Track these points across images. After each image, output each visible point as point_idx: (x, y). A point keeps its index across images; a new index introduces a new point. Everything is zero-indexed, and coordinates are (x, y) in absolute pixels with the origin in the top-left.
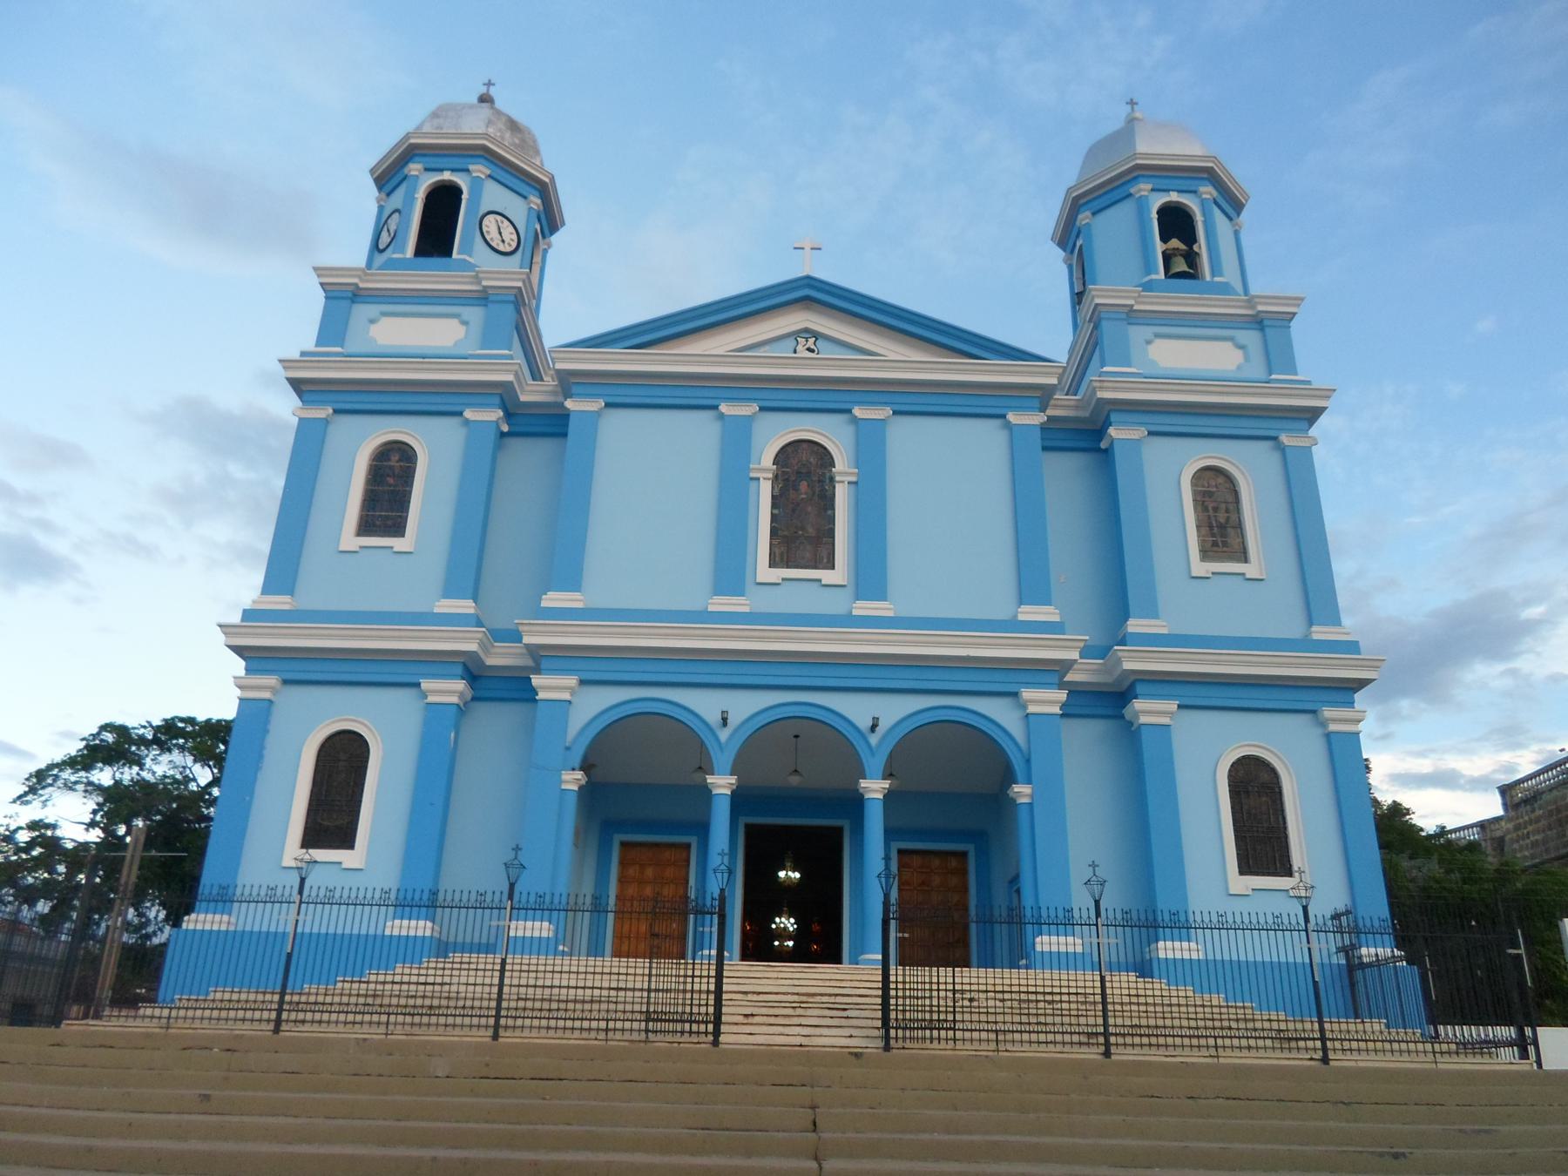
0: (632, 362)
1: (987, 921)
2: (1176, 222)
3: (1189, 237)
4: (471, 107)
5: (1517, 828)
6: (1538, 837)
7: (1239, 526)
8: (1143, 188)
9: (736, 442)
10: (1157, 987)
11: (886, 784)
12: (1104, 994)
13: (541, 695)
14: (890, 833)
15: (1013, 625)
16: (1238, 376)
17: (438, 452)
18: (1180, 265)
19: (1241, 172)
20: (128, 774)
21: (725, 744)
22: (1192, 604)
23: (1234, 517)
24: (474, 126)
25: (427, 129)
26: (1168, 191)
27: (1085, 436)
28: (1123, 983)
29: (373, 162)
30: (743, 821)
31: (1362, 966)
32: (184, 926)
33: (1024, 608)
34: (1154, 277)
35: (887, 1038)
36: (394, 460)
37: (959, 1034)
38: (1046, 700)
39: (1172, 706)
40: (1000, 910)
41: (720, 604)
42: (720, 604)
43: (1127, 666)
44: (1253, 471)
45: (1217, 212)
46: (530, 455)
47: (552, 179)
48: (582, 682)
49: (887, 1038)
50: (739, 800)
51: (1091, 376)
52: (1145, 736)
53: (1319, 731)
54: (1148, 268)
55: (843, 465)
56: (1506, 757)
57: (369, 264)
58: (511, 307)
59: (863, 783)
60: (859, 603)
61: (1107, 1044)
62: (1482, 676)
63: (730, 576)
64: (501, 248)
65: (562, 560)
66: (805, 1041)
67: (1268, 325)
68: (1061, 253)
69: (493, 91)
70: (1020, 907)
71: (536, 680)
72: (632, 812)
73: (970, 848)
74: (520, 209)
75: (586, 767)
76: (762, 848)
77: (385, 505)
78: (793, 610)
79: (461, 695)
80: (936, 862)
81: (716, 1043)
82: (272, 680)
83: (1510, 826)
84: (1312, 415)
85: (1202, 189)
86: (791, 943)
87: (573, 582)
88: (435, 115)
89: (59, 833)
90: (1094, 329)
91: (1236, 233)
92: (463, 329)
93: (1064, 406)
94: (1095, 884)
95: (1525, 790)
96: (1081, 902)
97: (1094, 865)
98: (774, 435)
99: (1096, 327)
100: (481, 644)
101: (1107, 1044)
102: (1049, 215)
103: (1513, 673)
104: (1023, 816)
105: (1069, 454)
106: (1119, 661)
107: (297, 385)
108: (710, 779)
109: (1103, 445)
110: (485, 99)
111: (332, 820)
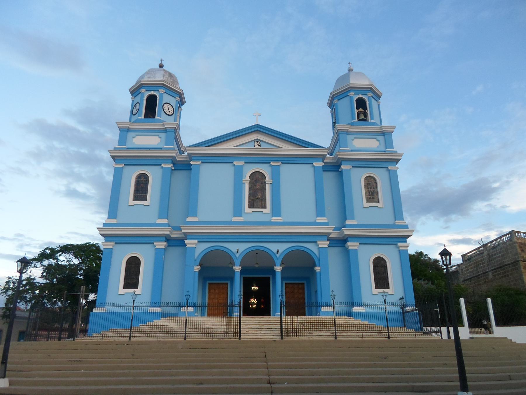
0: (208, 150)
1: (310, 306)
2: (361, 104)
3: (365, 108)
4: (156, 70)
5: (466, 267)
6: (471, 270)
7: (377, 193)
8: (352, 94)
10: (352, 319)
11: (281, 268)
12: (335, 322)
14: (283, 279)
15: (315, 223)
17: (155, 176)
18: (362, 117)
19: (379, 87)
20: (53, 262)
21: (238, 258)
22: (365, 215)
23: (375, 190)
24: (159, 77)
25: (146, 78)
27: (335, 167)
28: (342, 319)
30: (242, 276)
32: (94, 311)
33: (318, 218)
34: (354, 121)
35: (282, 335)
37: (299, 334)
38: (324, 244)
39: (358, 244)
40: (313, 301)
41: (236, 219)
42: (236, 219)
43: (346, 233)
45: (372, 99)
46: (181, 175)
47: (182, 91)
48: (198, 242)
49: (282, 335)
50: (242, 272)
51: (336, 151)
52: (351, 252)
53: (397, 249)
55: (268, 179)
56: (487, 234)
57: (130, 120)
59: (275, 268)
60: (273, 218)
61: (336, 335)
62: (480, 206)
64: (169, 114)
65: (191, 207)
67: (386, 134)
71: (186, 242)
72: (213, 275)
73: (305, 282)
74: (173, 101)
76: (247, 283)
77: (141, 193)
78: (255, 220)
79: (165, 246)
80: (296, 286)
81: (240, 339)
82: (113, 243)
83: (464, 267)
84: (397, 161)
85: (368, 94)
87: (195, 214)
88: (147, 73)
89: (35, 281)
91: (379, 105)
92: (160, 139)
93: (329, 159)
95: (490, 246)
98: (249, 170)
99: (338, 136)
100: (170, 232)
101: (336, 335)
103: (490, 205)
104: (318, 275)
105: (329, 173)
107: (113, 157)
109: (340, 170)
110: (161, 66)
111: (131, 281)
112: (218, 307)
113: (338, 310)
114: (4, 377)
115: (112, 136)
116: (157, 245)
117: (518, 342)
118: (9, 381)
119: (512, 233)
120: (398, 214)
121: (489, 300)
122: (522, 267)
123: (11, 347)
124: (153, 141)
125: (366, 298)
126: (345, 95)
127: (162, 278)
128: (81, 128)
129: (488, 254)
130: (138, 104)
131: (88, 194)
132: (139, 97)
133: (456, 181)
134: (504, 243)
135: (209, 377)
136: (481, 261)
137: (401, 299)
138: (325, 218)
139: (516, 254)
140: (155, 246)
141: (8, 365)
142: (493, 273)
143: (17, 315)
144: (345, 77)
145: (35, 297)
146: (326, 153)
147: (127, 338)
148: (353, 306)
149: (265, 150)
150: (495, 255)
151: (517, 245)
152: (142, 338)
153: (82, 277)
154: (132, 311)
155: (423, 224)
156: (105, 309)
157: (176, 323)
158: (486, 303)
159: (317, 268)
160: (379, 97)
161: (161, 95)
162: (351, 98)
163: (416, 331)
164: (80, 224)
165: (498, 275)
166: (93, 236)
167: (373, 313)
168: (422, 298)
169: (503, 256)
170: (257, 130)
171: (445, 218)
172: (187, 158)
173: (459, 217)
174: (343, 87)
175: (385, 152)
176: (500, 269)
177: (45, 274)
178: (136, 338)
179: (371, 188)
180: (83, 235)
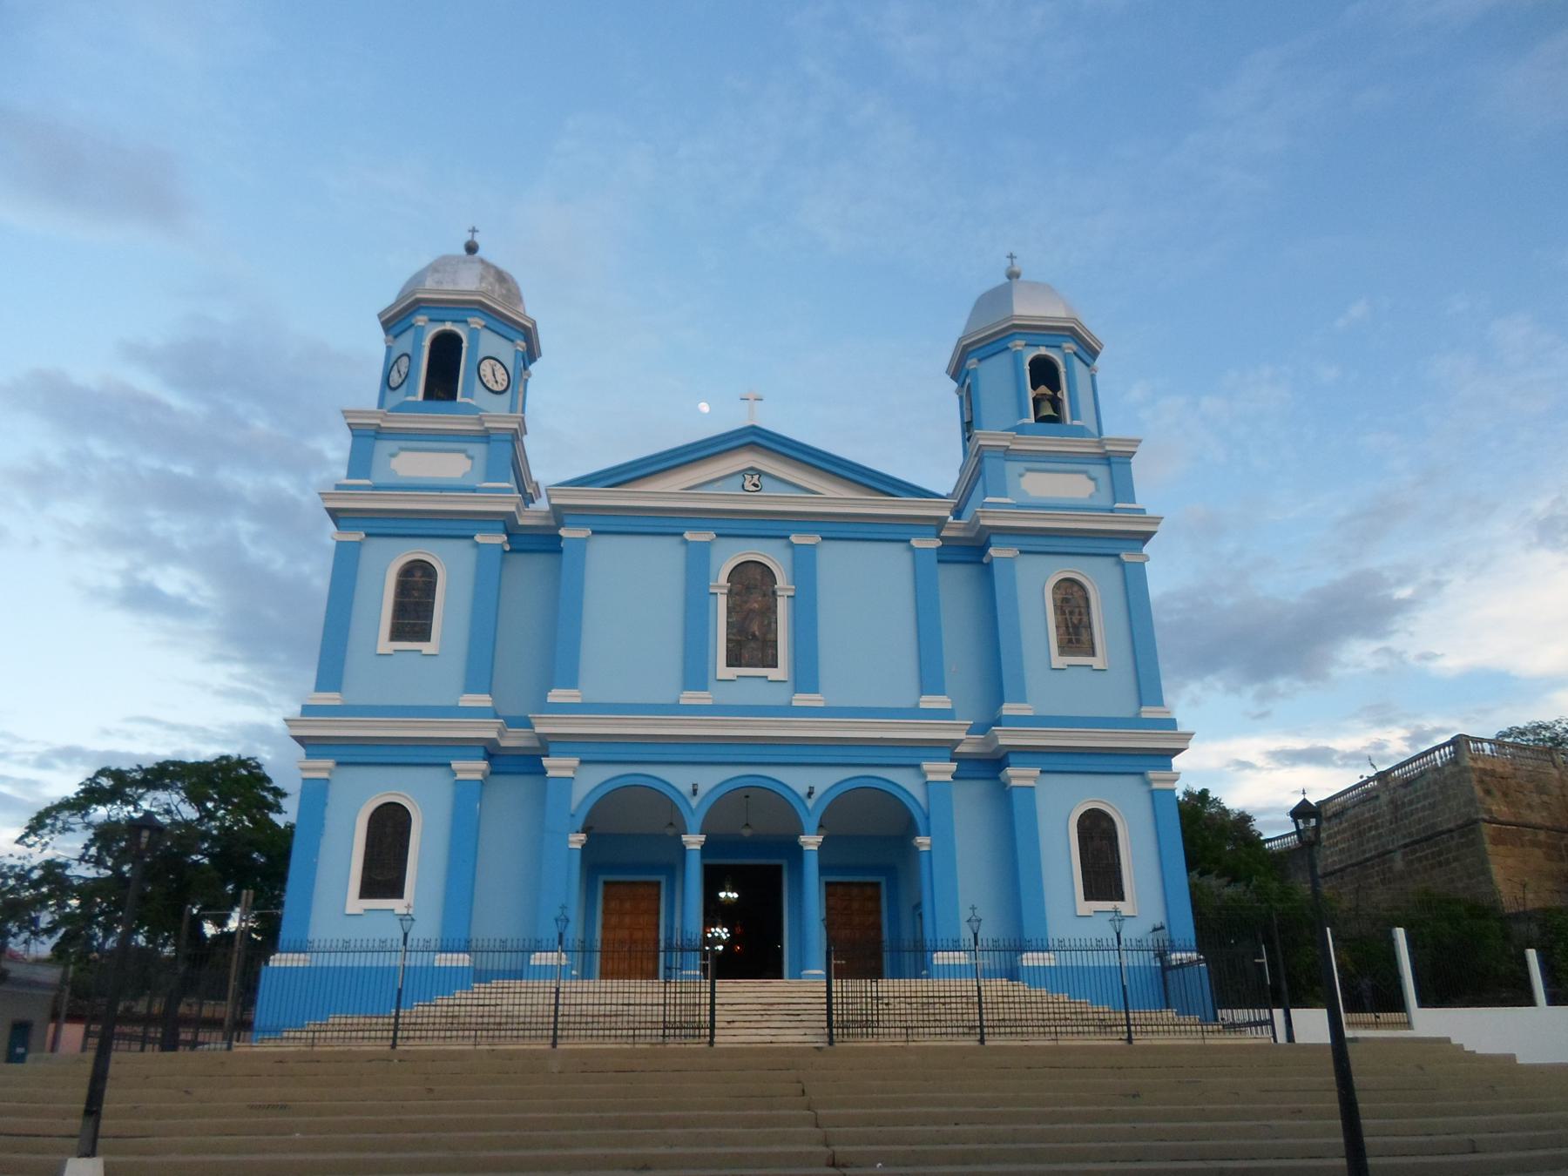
1: (897, 950)
2: (1044, 372)
3: (1055, 385)
7: (1089, 626)
8: (1018, 344)
9: (698, 563)
10: (1021, 988)
11: (820, 839)
12: (979, 996)
13: (550, 773)
14: (823, 869)
15: (916, 712)
16: (1095, 503)
17: (453, 568)
18: (1047, 411)
19: (1095, 326)
21: (695, 811)
22: (1057, 691)
23: (1085, 619)
24: (468, 282)
26: (443, 321)
27: (970, 551)
28: (995, 987)
29: (381, 308)
31: (1172, 968)
33: (924, 698)
34: (1026, 421)
35: (830, 1035)
36: (418, 576)
38: (941, 770)
39: (1036, 772)
40: (907, 935)
41: (690, 698)
42: (690, 698)
43: (1002, 742)
44: (1099, 579)
45: (1076, 361)
46: (529, 571)
47: (534, 324)
48: (582, 762)
50: (706, 849)
52: (1016, 795)
53: (1145, 788)
54: (1022, 413)
55: (782, 582)
56: (1377, 735)
57: (381, 405)
58: (509, 445)
59: (803, 839)
60: (797, 696)
61: (982, 1034)
62: (1357, 655)
63: (695, 675)
64: (496, 388)
65: (559, 657)
66: (774, 1039)
67: (1114, 462)
68: (955, 385)
69: (478, 239)
70: (922, 939)
71: (546, 762)
72: (623, 865)
73: (882, 880)
74: (507, 351)
75: (586, 830)
76: (714, 878)
77: (412, 616)
78: (746, 699)
81: (711, 1043)
84: (1146, 537)
85: (1065, 345)
86: (720, 948)
87: (572, 683)
88: (434, 268)
89: (68, 872)
90: (976, 472)
91: (1093, 377)
92: (469, 462)
94: (975, 921)
96: (966, 934)
97: (973, 908)
98: (727, 557)
100: (500, 733)
101: (982, 1034)
102: (945, 355)
106: (996, 738)
107: (334, 514)
108: (684, 838)
110: (471, 248)
111: (383, 875)
112: (629, 949)
113: (985, 961)
114: (91, 1153)
115: (335, 449)
116: (463, 771)
117: (1479, 1051)
118: (106, 1165)
119: (1459, 742)
120: (1147, 686)
121: (1400, 934)
122: (1487, 839)
123: (112, 1069)
124: (450, 466)
125: (1057, 929)
126: (997, 347)
127: (475, 866)
128: (175, 400)
129: (1392, 802)
130: (405, 359)
131: (193, 600)
132: (407, 338)
133: (1289, 579)
134: (1436, 769)
135: (662, 1150)
136: (1373, 819)
137: (1155, 930)
138: (944, 698)
139: (1471, 801)
140: (454, 773)
141: (103, 1123)
142: (1405, 854)
143: (12, 975)
144: (998, 297)
145: (67, 919)
146: (947, 513)
147: (385, 1042)
148: (1020, 948)
149: (773, 500)
150: (1411, 803)
151: (1474, 777)
152: (429, 1041)
153: (206, 861)
154: (399, 963)
155: (1195, 702)
156: (308, 956)
157: (525, 999)
158: (1391, 942)
159: (923, 842)
160: (1094, 354)
161: (474, 334)
162: (1017, 357)
163: (1204, 1021)
164: (194, 700)
165: (1420, 860)
166: (204, 730)
167: (1083, 970)
168: (1214, 927)
169: (1433, 806)
170: (753, 443)
171: (1258, 686)
172: (547, 518)
173: (1300, 684)
174: (993, 322)
175: (1112, 511)
176: (1424, 845)
177: (93, 851)
178: (411, 1042)
179: (1071, 613)
180: (173, 727)
